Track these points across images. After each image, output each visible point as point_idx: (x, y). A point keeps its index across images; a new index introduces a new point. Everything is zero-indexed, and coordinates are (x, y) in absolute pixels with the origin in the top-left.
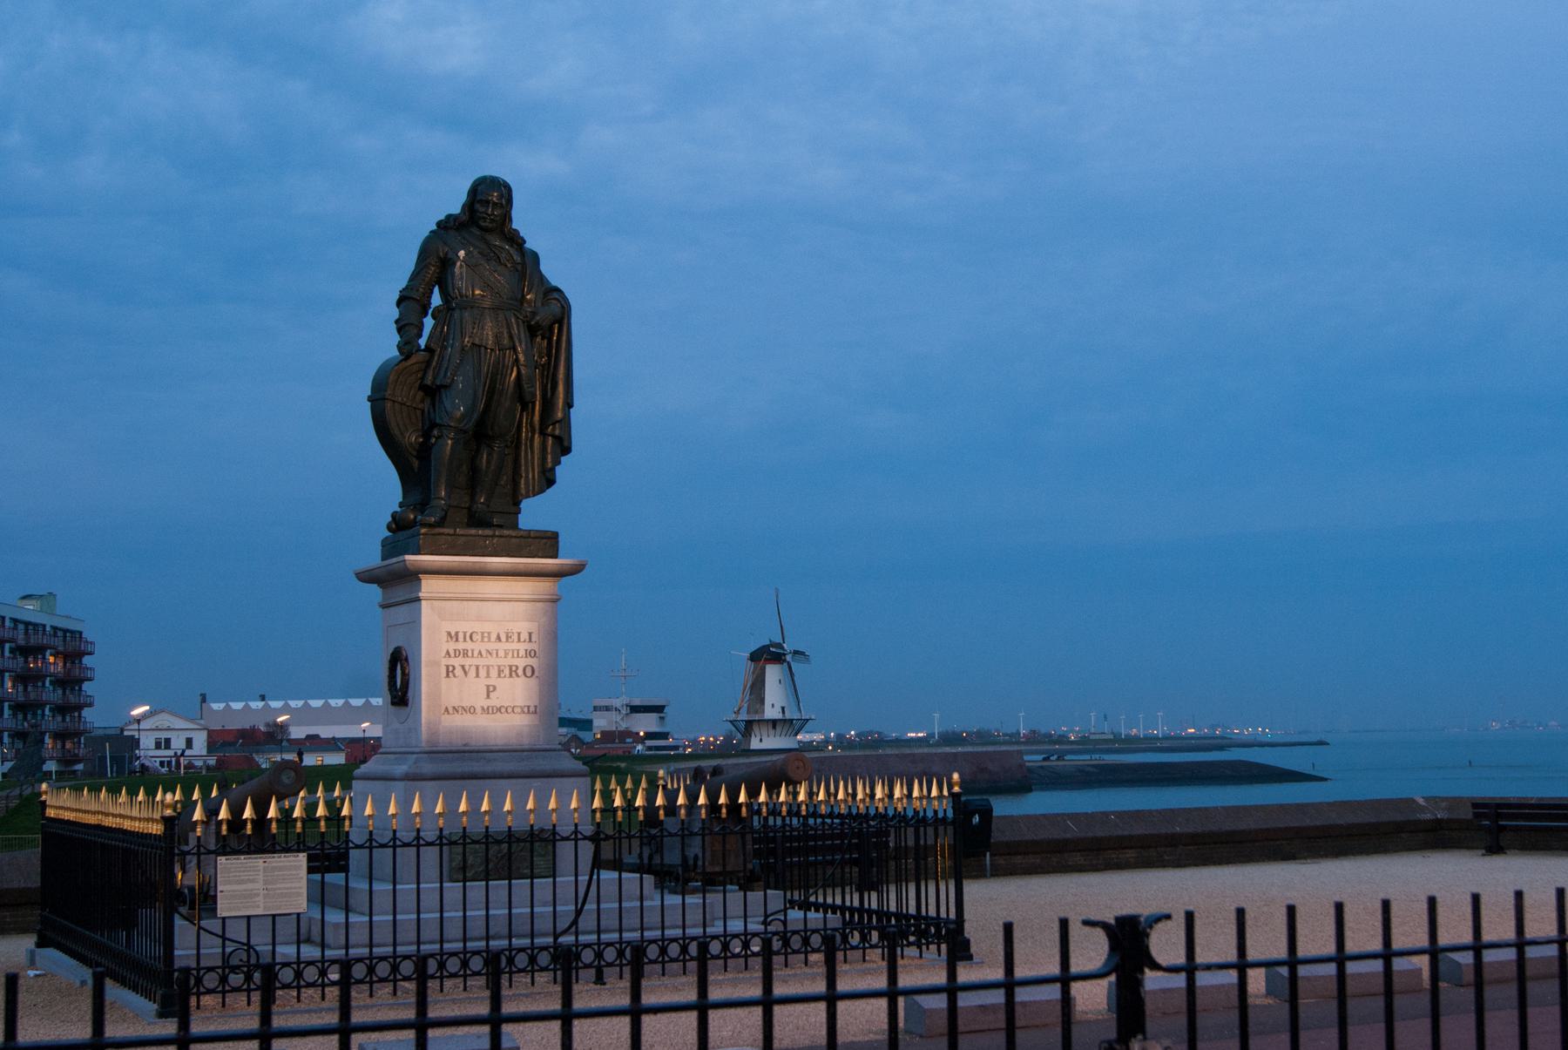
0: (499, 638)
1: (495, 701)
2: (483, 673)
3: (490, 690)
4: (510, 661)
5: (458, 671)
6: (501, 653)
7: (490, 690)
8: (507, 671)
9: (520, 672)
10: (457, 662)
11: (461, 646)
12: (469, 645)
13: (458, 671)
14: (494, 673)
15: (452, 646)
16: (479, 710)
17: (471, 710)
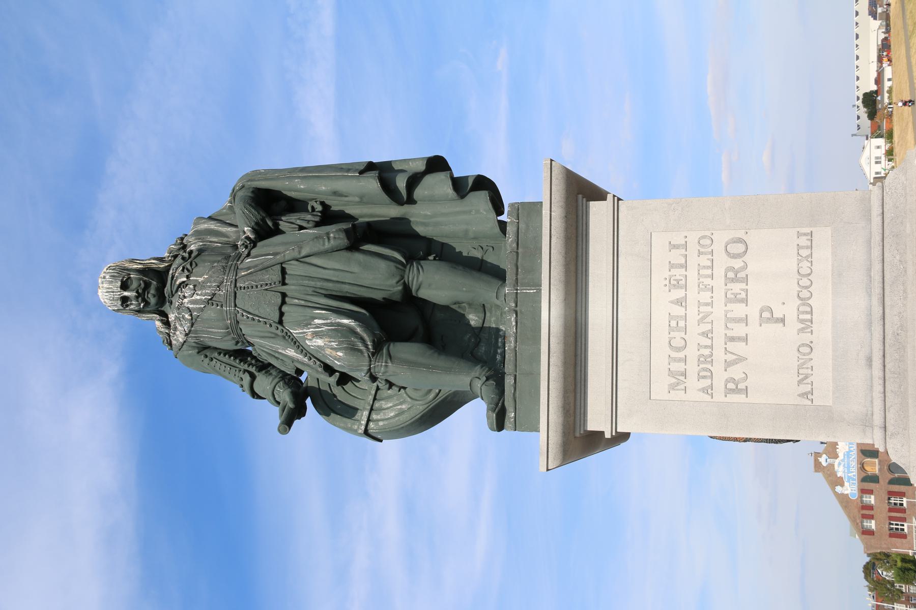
0: (681, 302)
1: (790, 310)
2: (739, 330)
3: (769, 317)
5: (736, 372)
7: (769, 317)
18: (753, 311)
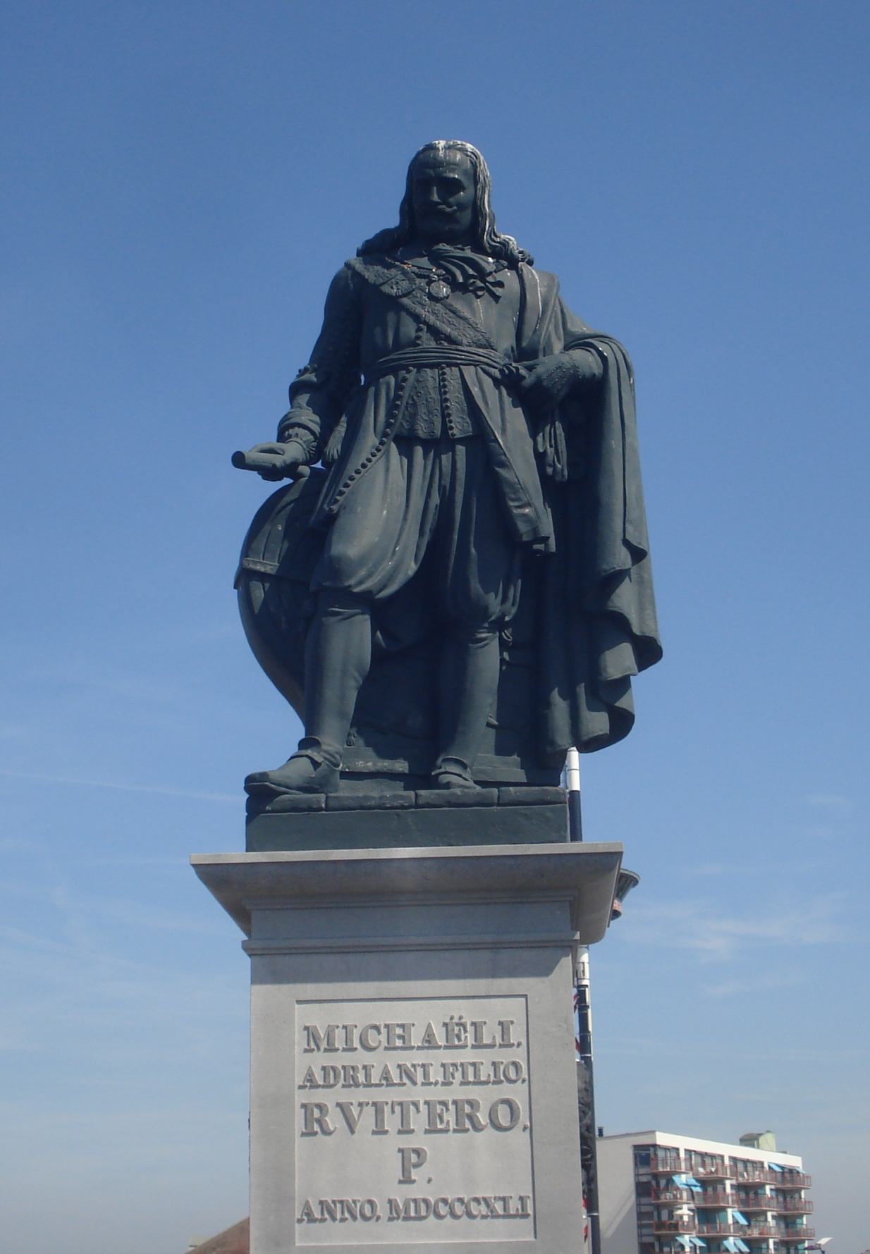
1: (418, 1191)
2: (392, 1122)
3: (411, 1160)
4: (457, 1092)
5: (334, 1120)
6: (436, 1075)
7: (411, 1160)
8: (450, 1117)
9: (482, 1118)
10: (329, 1098)
11: (340, 1060)
12: (361, 1058)
13: (334, 1120)
14: (419, 1121)
15: (320, 1060)
16: (383, 1210)
17: (362, 1212)
18: (418, 1140)
